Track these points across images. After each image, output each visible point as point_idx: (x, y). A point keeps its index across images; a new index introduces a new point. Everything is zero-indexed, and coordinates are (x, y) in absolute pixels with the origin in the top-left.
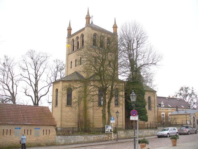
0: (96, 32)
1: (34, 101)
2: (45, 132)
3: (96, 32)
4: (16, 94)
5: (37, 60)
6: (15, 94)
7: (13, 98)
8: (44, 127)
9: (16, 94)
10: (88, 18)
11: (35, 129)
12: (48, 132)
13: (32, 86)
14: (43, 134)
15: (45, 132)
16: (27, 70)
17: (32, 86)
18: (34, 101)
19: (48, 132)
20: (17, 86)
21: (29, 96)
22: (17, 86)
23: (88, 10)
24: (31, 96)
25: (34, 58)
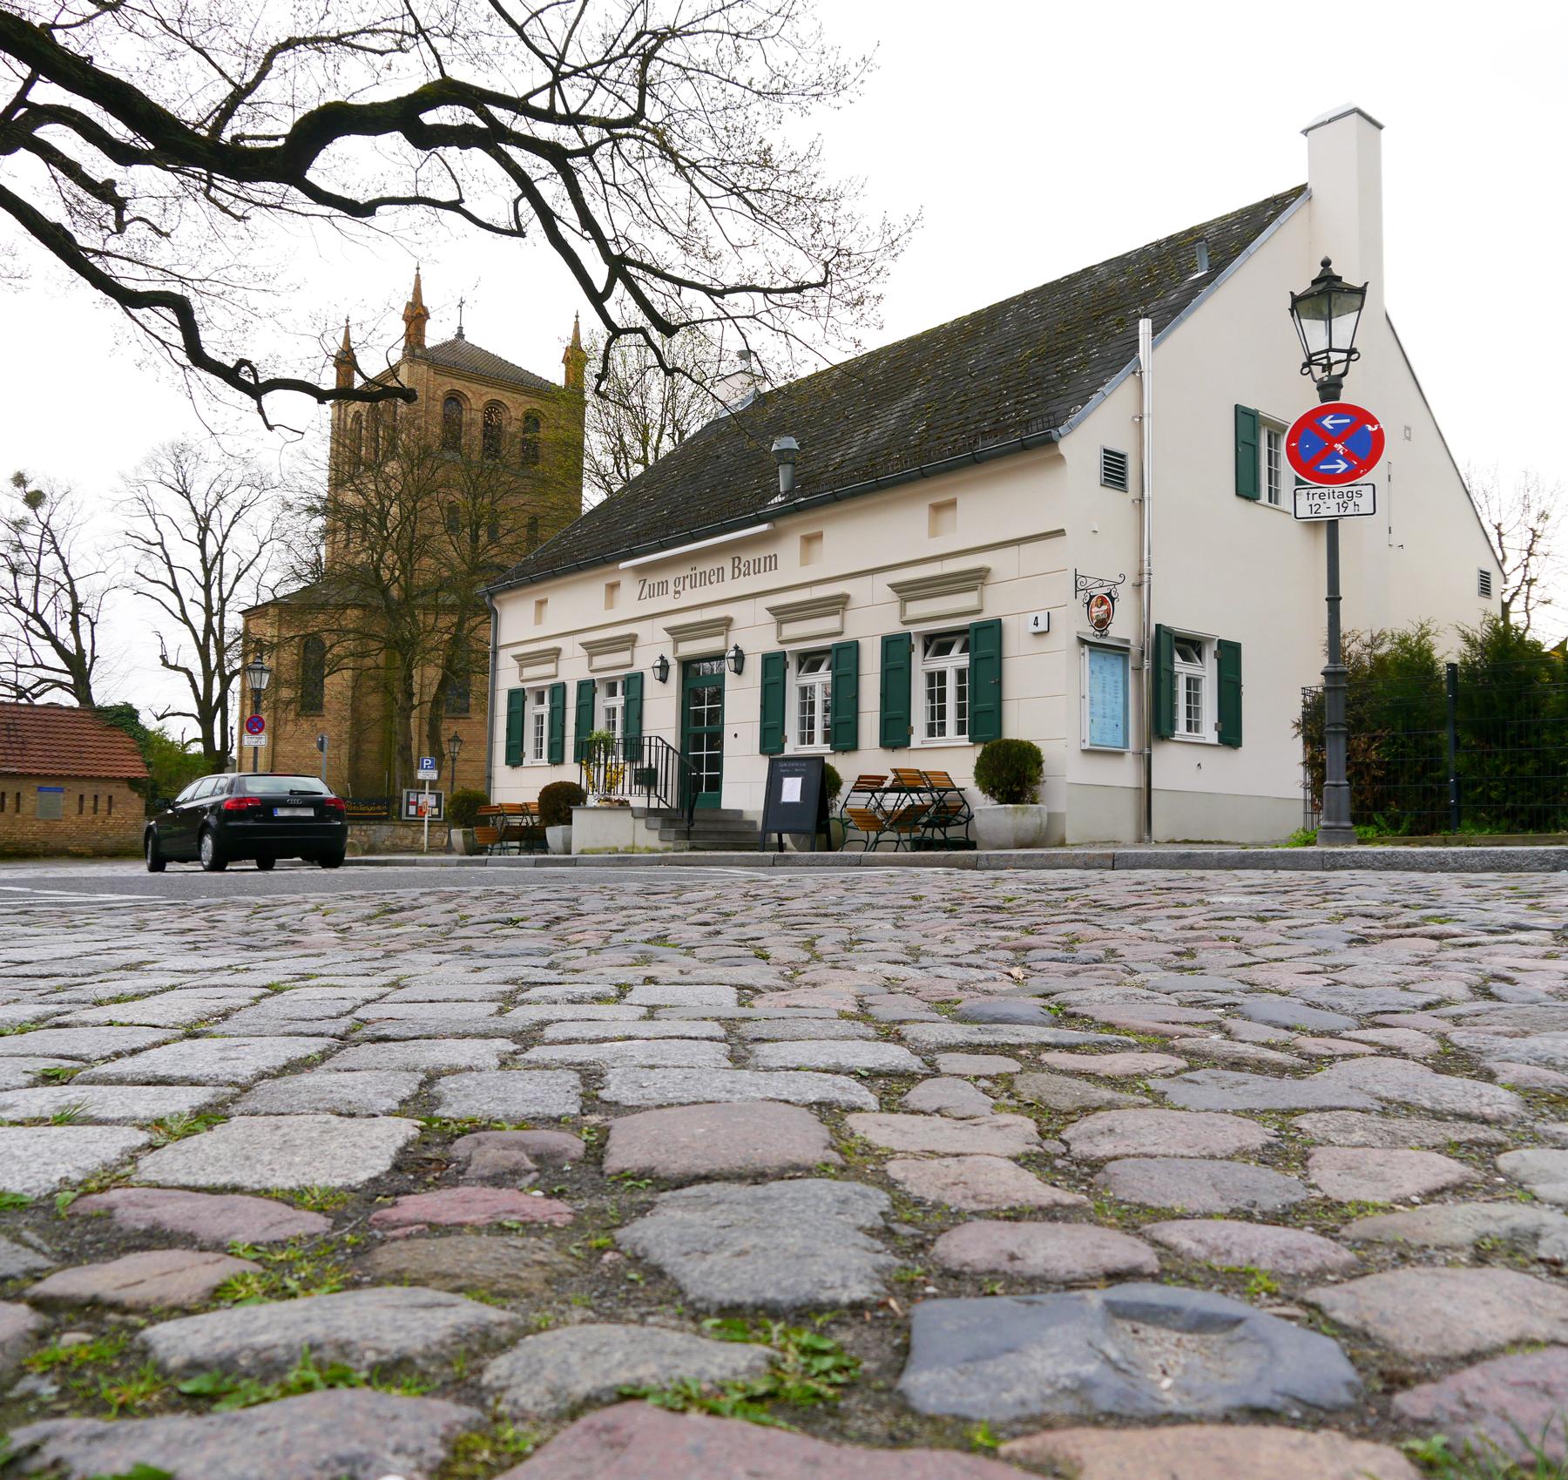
0: (536, 405)
1: (201, 692)
2: (89, 803)
3: (536, 405)
4: (93, 658)
5: (212, 499)
6: (88, 660)
7: (79, 666)
8: (85, 784)
9: (93, 658)
10: (1326, 263)
11: (40, 789)
12: (103, 804)
13: (186, 621)
14: (81, 812)
15: (89, 803)
16: (161, 544)
17: (186, 621)
18: (201, 692)
19: (103, 804)
20: (93, 624)
21: (176, 668)
22: (93, 624)
23: (418, 276)
24: (186, 671)
25: (197, 491)
